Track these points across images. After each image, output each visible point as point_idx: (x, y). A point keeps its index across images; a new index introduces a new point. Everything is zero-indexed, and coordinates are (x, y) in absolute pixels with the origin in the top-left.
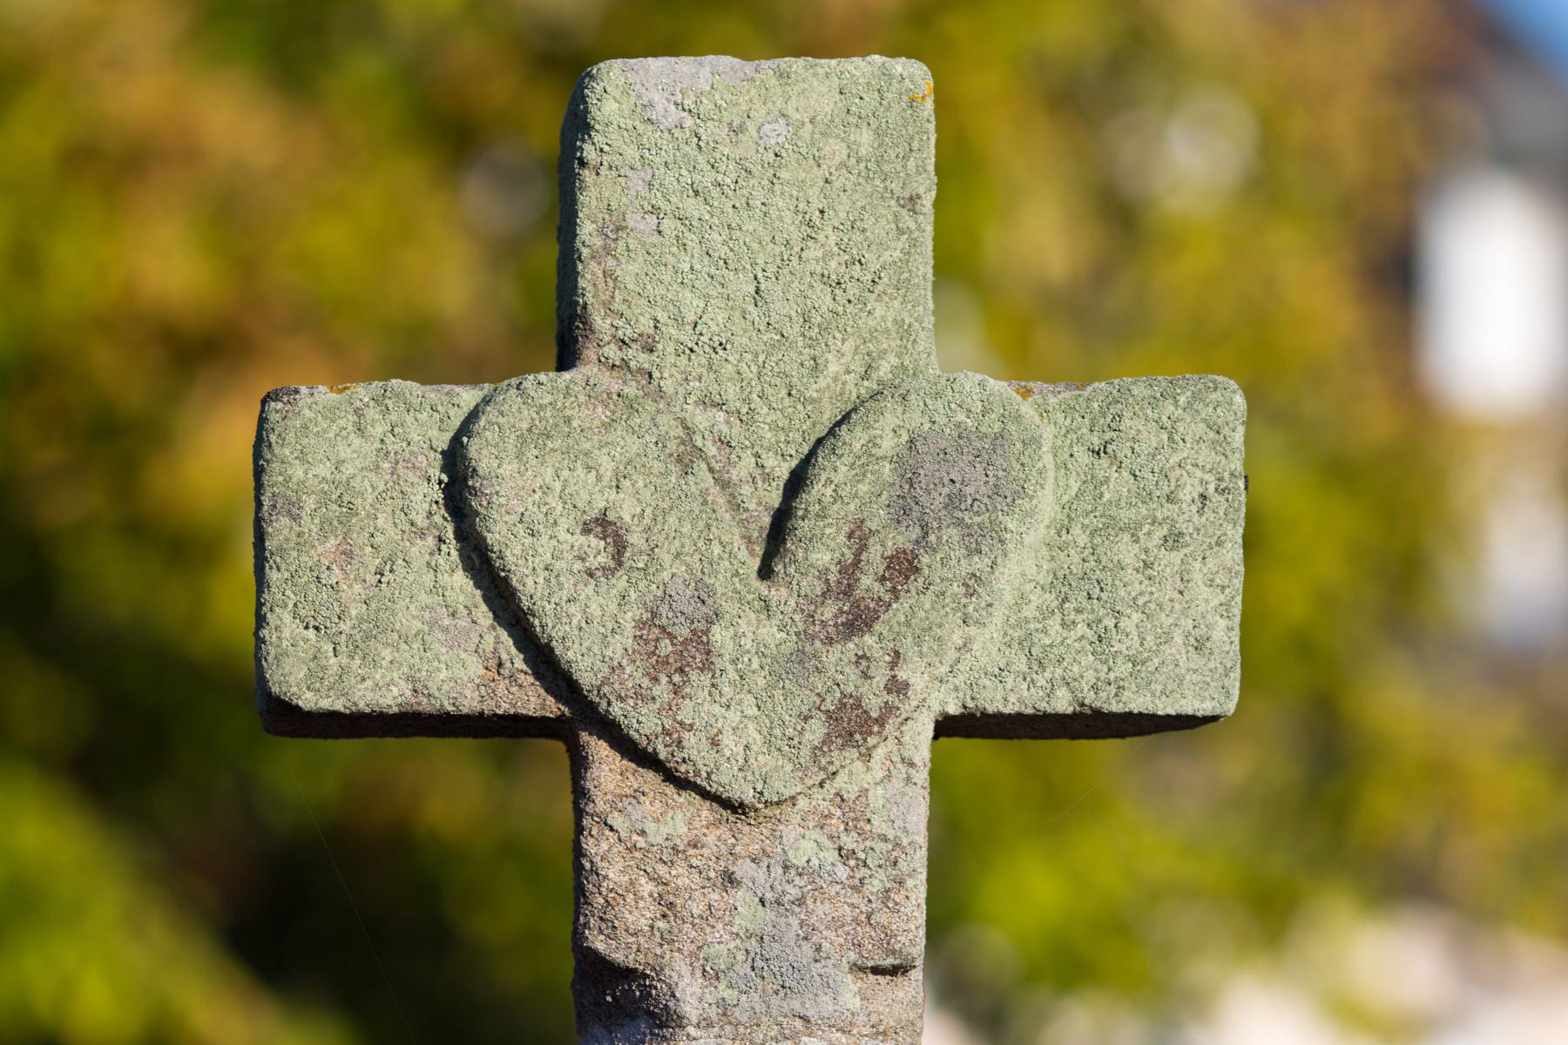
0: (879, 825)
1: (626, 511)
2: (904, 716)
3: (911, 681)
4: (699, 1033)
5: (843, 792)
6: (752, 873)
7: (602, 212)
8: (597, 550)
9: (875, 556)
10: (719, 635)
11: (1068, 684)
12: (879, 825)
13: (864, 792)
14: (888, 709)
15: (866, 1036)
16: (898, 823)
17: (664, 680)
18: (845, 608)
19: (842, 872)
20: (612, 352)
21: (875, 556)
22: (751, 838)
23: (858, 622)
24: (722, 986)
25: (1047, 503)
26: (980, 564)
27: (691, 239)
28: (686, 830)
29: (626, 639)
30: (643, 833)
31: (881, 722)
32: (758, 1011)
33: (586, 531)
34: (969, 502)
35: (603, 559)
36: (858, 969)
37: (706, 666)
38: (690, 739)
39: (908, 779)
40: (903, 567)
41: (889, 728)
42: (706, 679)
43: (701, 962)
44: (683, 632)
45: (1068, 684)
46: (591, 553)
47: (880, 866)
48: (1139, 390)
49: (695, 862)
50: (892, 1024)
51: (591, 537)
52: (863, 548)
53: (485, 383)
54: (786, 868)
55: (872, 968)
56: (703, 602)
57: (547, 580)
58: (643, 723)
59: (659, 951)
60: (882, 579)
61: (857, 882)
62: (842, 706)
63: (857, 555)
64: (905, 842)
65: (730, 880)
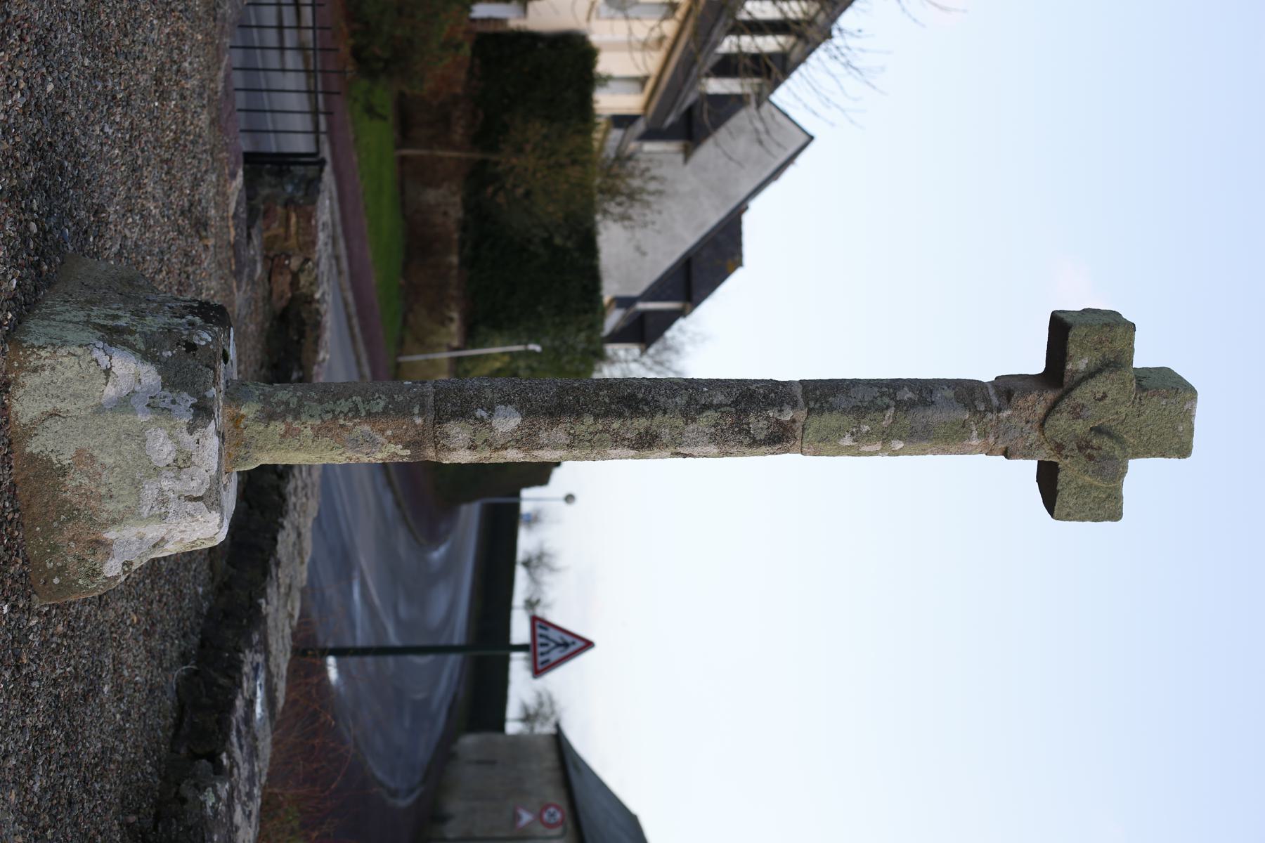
1: (1107, 401)
8: (1099, 396)
9: (1095, 453)
10: (1081, 421)
13: (1044, 449)
19: (1027, 444)
21: (1095, 453)
22: (1036, 426)
23: (1080, 448)
25: (153, 532)
29: (1078, 400)
33: (1103, 393)
38: (1059, 415)
40: (1091, 457)
48: (167, 747)
53: (742, 6)
54: (1029, 433)
65: (1027, 422)
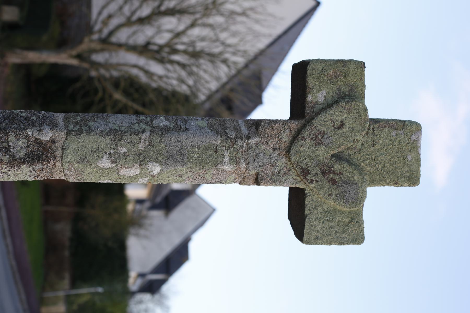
0: (285, 178)
2: (306, 183)
3: (313, 184)
4: (204, 139)
5: (291, 171)
6: (276, 153)
7: (232, 157)
8: (337, 124)
11: (310, 213)
12: (285, 178)
14: (307, 180)
15: (244, 175)
16: (285, 181)
17: (314, 137)
18: (327, 171)
19: (276, 171)
20: (372, 127)
21: (336, 178)
24: (255, 147)
26: (334, 196)
27: (391, 142)
28: (284, 140)
30: (284, 132)
31: (305, 178)
32: (250, 154)
33: (341, 122)
34: (346, 195)
35: (336, 125)
36: (257, 174)
37: (316, 145)
38: (302, 141)
39: (293, 183)
40: (333, 182)
41: (304, 180)
42: (314, 144)
43: (259, 143)
44: (323, 140)
45: (310, 213)
46: (337, 123)
47: (277, 178)
49: (278, 142)
50: (246, 180)
51: (340, 123)
52: (338, 175)
54: (277, 160)
55: (258, 177)
56: (328, 144)
57: (332, 114)
58: (306, 133)
59: (261, 135)
60: (332, 178)
61: (274, 173)
62: (308, 171)
63: (336, 174)
64: (282, 183)
